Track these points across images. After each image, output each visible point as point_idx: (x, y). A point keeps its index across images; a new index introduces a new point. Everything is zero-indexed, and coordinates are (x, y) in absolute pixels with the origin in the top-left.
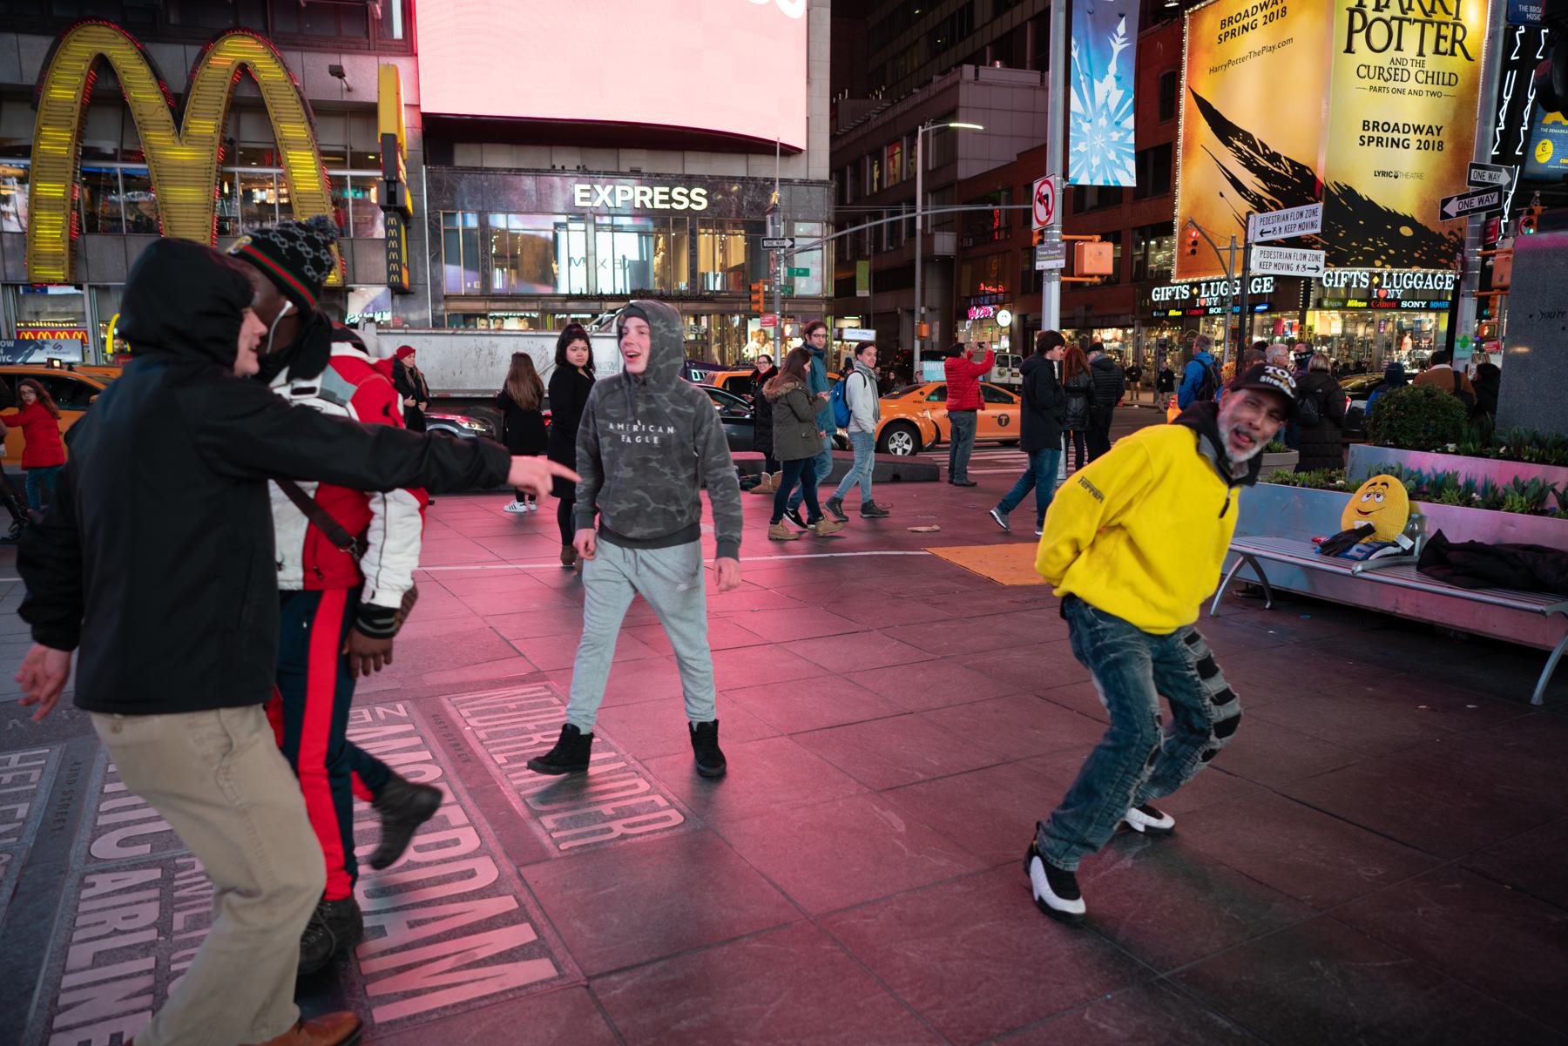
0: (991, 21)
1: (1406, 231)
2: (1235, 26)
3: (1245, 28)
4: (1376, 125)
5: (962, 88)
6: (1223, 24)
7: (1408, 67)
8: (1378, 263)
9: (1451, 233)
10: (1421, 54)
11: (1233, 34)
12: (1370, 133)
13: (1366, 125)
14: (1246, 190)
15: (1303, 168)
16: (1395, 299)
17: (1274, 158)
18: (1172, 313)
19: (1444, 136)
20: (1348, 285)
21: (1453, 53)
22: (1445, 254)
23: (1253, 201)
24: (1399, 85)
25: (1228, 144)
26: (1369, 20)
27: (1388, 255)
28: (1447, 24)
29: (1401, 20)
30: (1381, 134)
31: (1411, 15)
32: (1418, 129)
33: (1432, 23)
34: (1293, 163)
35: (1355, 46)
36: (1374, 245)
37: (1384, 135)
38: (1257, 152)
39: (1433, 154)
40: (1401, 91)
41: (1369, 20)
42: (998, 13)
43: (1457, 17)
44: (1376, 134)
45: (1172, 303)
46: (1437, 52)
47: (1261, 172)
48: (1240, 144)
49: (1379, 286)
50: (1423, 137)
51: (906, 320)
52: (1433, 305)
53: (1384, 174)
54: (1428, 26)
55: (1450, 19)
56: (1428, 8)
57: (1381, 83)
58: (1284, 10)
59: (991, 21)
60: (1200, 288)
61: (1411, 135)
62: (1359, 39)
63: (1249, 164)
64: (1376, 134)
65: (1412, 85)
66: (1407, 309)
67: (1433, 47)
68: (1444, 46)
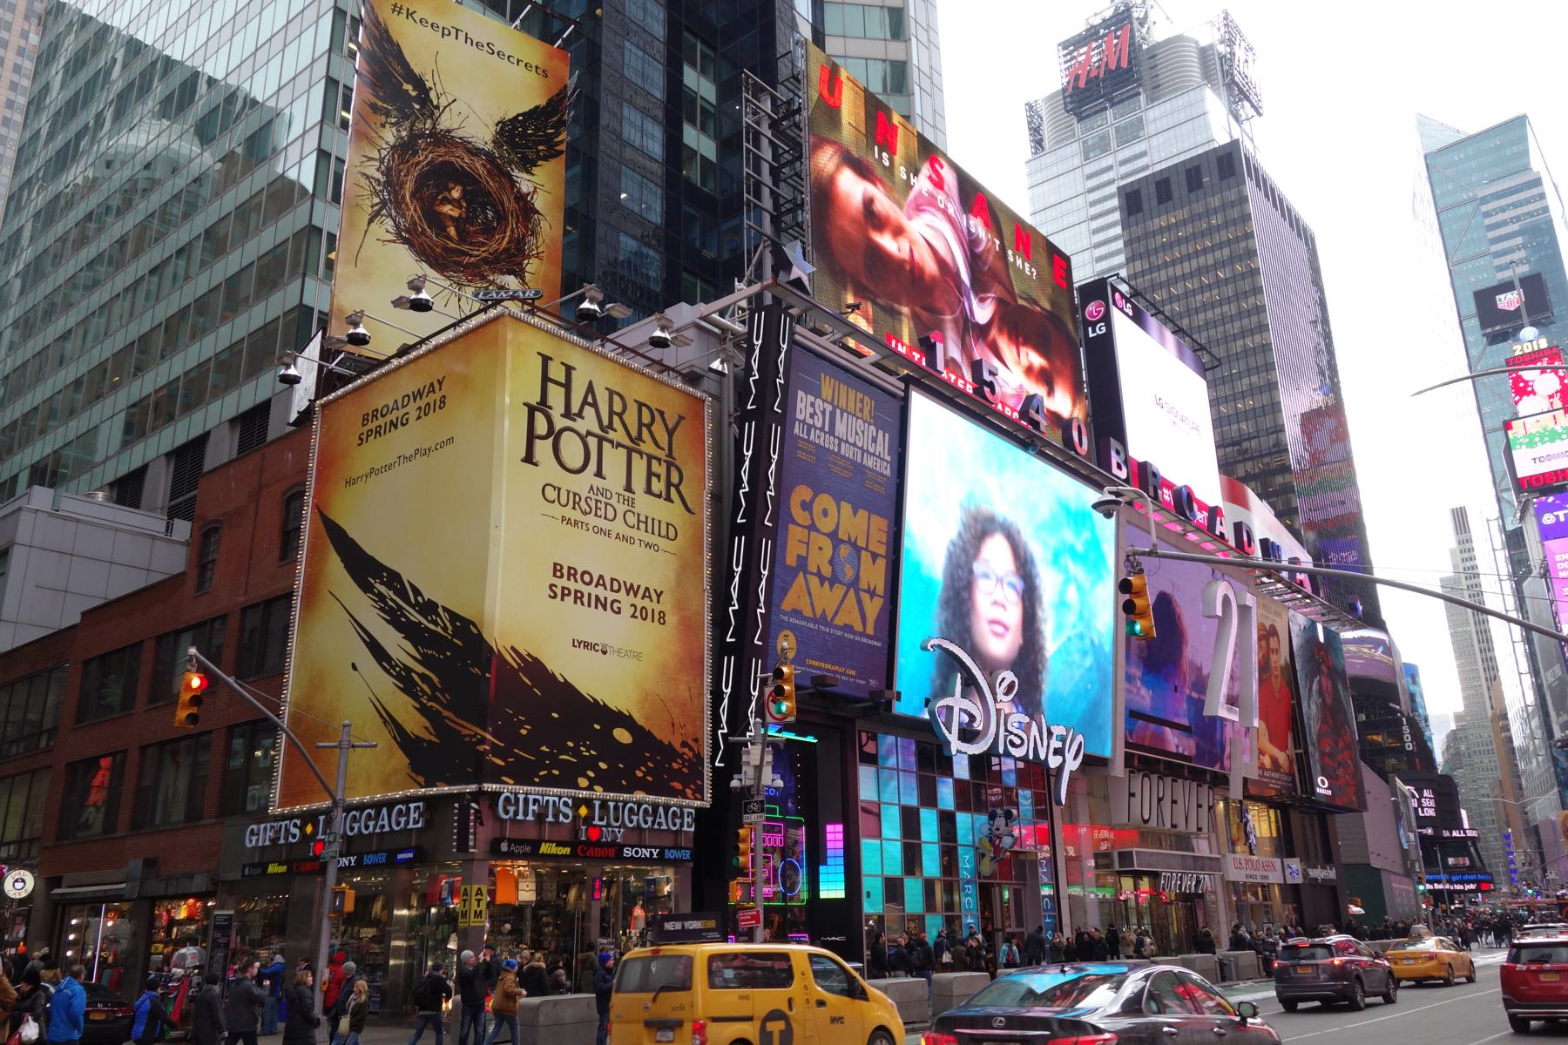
0: (118, 453)
1: (622, 735)
2: (381, 421)
3: (394, 425)
4: (572, 572)
5: (25, 518)
6: (365, 420)
7: (614, 501)
8: (583, 782)
9: (684, 744)
10: (629, 488)
11: (378, 432)
12: (564, 582)
13: (557, 569)
14: (388, 659)
15: (467, 623)
16: (613, 844)
17: (429, 608)
18: (273, 869)
19: (666, 604)
20: (540, 817)
21: (668, 499)
22: (677, 775)
23: (398, 677)
24: (602, 523)
25: (367, 588)
26: (558, 427)
27: (596, 769)
28: (659, 460)
29: (601, 440)
30: (580, 586)
31: (611, 435)
32: (631, 590)
33: (641, 453)
34: (454, 616)
35: (538, 456)
36: (575, 752)
37: (586, 589)
38: (406, 599)
39: (651, 627)
40: (607, 533)
41: (558, 427)
42: (126, 444)
43: (670, 455)
44: (572, 585)
45: (272, 851)
46: (649, 491)
47: (411, 631)
48: (383, 589)
49: (588, 820)
50: (640, 603)
51: (1022, 857)
52: (669, 854)
53: (587, 645)
54: (635, 456)
55: (662, 454)
56: (634, 434)
57: (576, 515)
58: (443, 400)
59: (118, 453)
60: (315, 827)
61: (622, 595)
62: (543, 448)
63: (395, 618)
64: (572, 585)
65: (618, 526)
66: (632, 860)
67: (643, 484)
68: (658, 486)
